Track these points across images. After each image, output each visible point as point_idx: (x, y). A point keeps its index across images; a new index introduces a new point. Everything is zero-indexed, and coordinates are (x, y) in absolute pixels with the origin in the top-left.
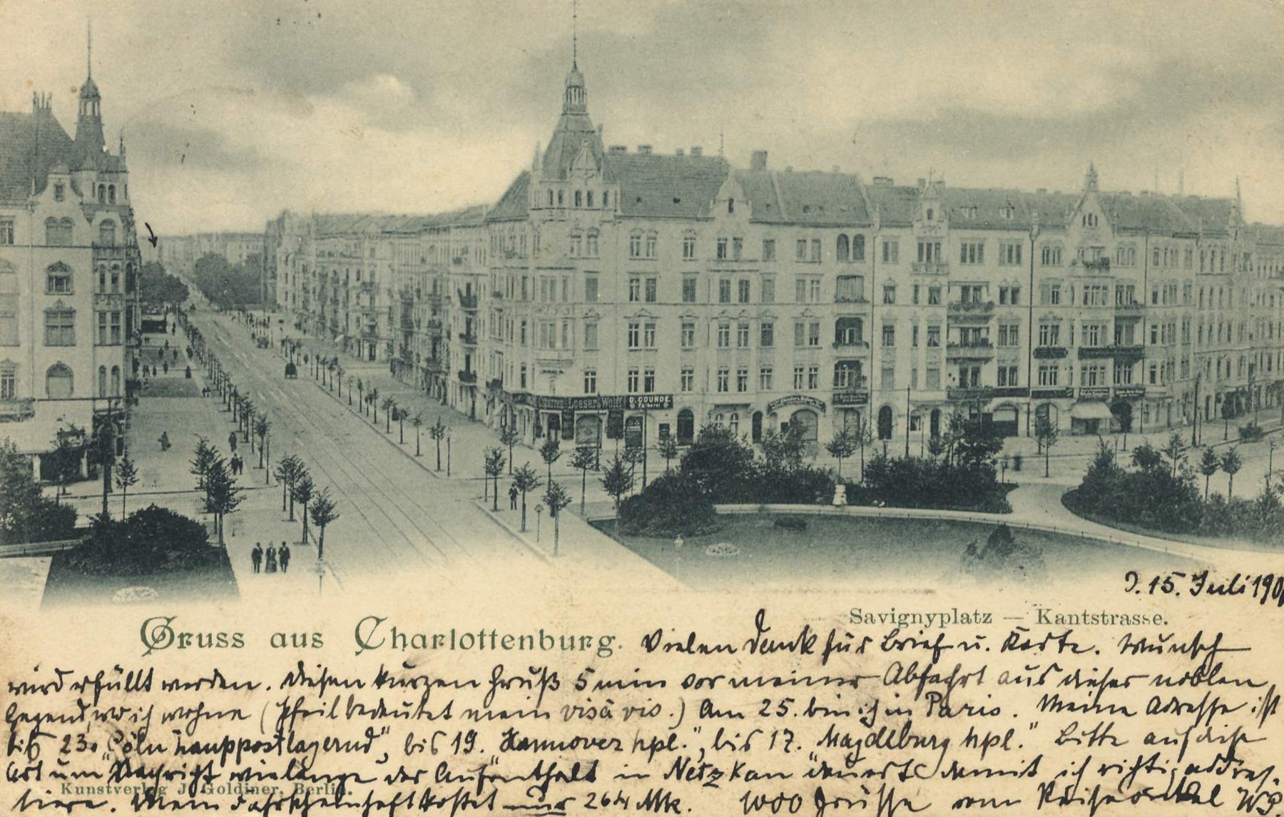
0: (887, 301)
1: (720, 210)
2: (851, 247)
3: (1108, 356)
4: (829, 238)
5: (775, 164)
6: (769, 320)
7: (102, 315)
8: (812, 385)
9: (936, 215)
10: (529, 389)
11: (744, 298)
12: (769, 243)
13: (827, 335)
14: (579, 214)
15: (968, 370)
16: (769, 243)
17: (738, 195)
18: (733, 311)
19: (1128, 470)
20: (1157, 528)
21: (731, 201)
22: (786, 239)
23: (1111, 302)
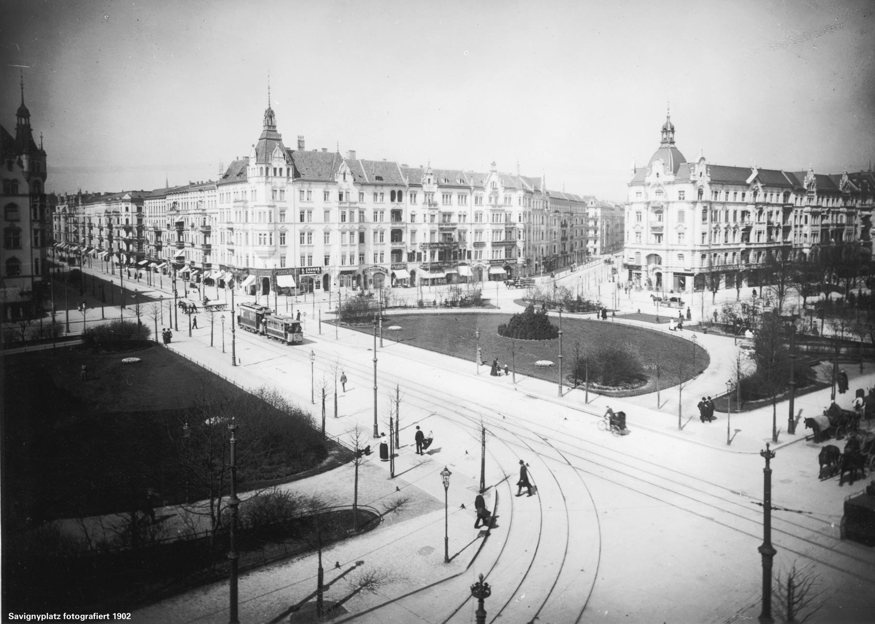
0: (412, 221)
1: (339, 179)
2: (397, 196)
3: (502, 246)
4: (387, 191)
5: (569, 271)
6: (362, 230)
7: (36, 231)
8: (382, 261)
9: (432, 181)
10: (250, 266)
11: (352, 219)
12: (361, 194)
13: (388, 236)
14: (275, 180)
15: (139, 209)
16: (361, 194)
17: (348, 171)
18: (347, 227)
19: (56, 521)
20: (358, 534)
21: (344, 174)
22: (368, 192)
23: (503, 221)
